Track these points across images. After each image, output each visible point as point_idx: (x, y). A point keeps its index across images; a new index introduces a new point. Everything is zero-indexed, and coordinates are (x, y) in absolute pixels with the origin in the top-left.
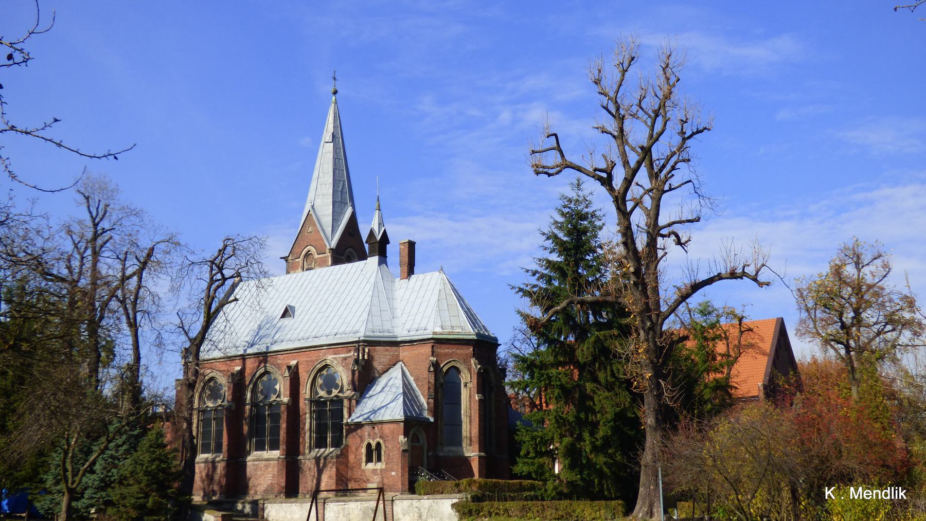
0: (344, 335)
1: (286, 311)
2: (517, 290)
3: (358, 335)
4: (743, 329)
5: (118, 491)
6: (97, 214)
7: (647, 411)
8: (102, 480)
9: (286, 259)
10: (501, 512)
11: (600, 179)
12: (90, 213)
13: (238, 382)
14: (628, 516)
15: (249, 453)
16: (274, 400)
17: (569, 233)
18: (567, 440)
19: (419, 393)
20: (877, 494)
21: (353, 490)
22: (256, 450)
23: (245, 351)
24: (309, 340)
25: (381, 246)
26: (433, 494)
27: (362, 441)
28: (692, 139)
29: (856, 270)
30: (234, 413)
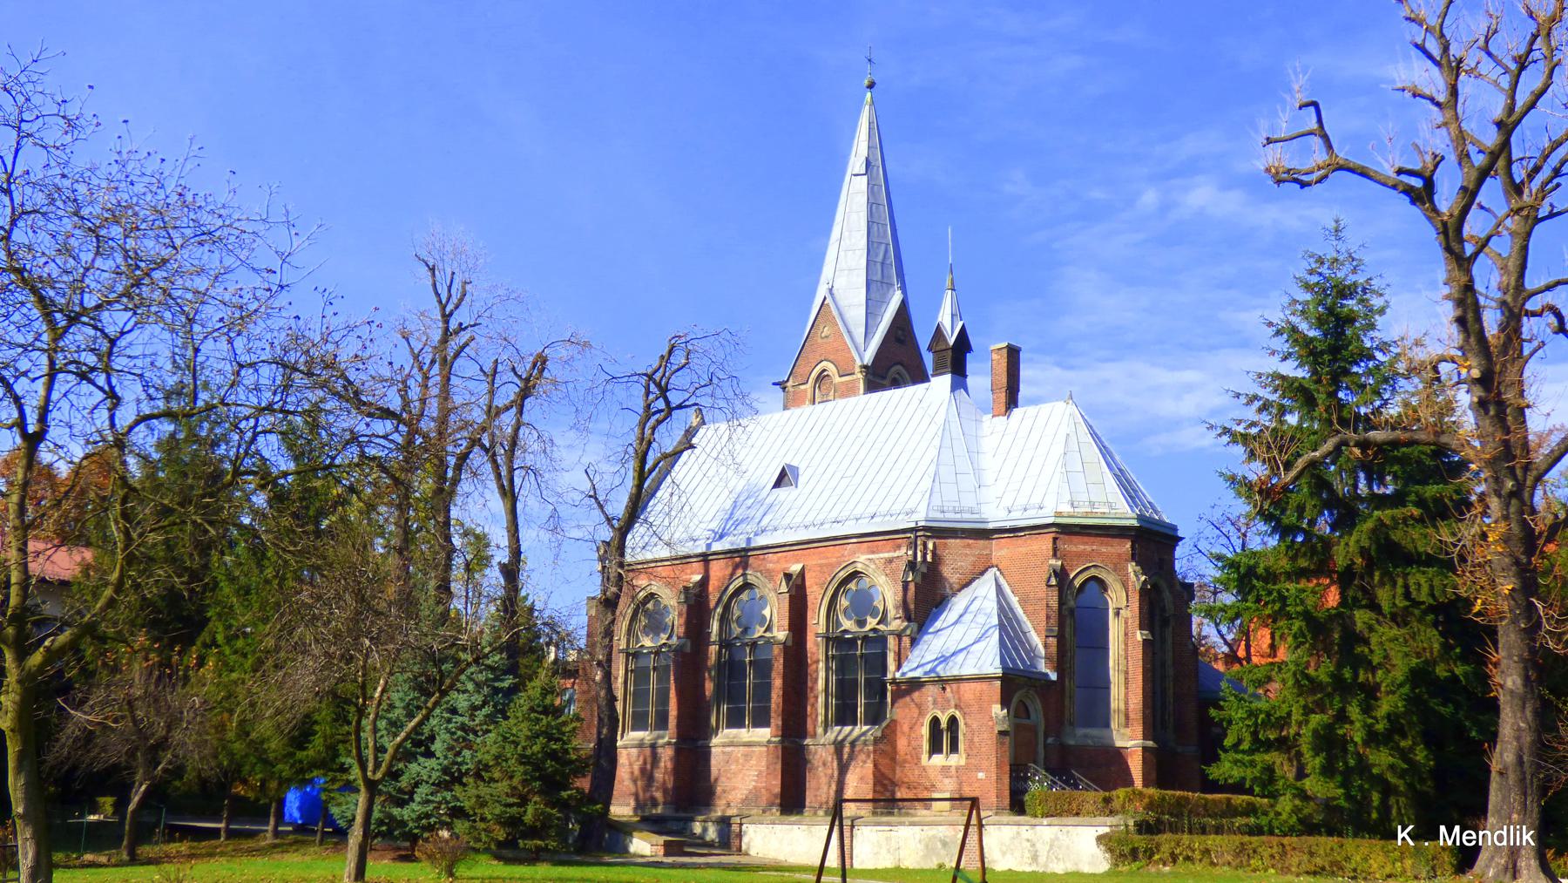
0: (887, 518)
1: (783, 475)
2: (1219, 431)
3: (915, 517)
5: (472, 791)
6: (450, 296)
7: (1504, 662)
8: (445, 771)
10: (1197, 855)
11: (1409, 191)
12: (438, 295)
13: (697, 602)
17: (1320, 322)
18: (1316, 719)
19: (1028, 625)
22: (728, 727)
23: (709, 546)
24: (825, 526)
25: (956, 358)
26: (1060, 815)
27: (921, 714)
30: (689, 660)
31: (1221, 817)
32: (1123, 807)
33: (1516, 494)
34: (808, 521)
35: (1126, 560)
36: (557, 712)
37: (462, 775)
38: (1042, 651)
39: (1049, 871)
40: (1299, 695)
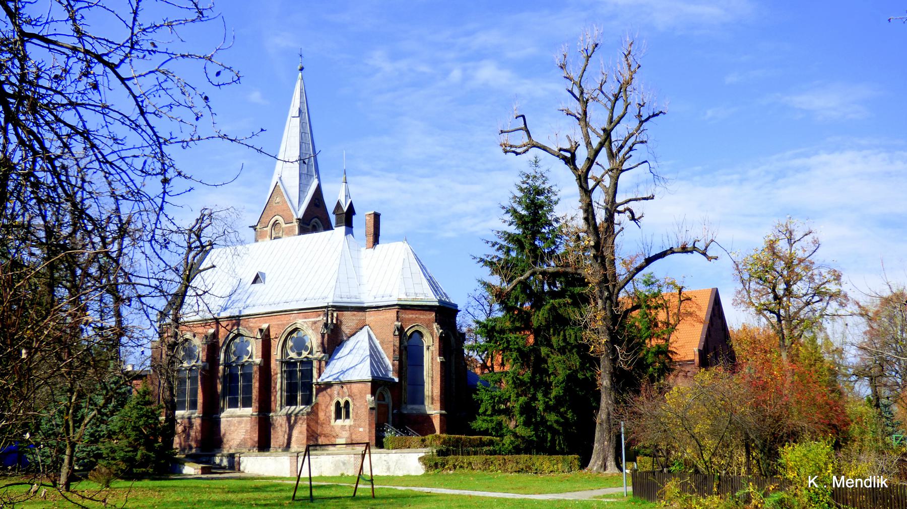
2: (479, 260)
4: (682, 299)
7: (602, 374)
9: (254, 227)
10: (465, 465)
11: (564, 158)
13: (212, 346)
14: (584, 469)
15: (223, 410)
16: (247, 361)
17: (527, 208)
18: (522, 399)
19: (384, 355)
20: (859, 483)
21: (322, 445)
22: (229, 407)
23: (219, 314)
25: (347, 217)
27: (331, 399)
28: (648, 122)
29: (788, 244)
31: (477, 447)
32: (431, 443)
33: (609, 298)
34: (271, 301)
35: (433, 322)
36: (149, 403)
37: (100, 437)
38: (391, 367)
39: (395, 475)
40: (514, 388)
